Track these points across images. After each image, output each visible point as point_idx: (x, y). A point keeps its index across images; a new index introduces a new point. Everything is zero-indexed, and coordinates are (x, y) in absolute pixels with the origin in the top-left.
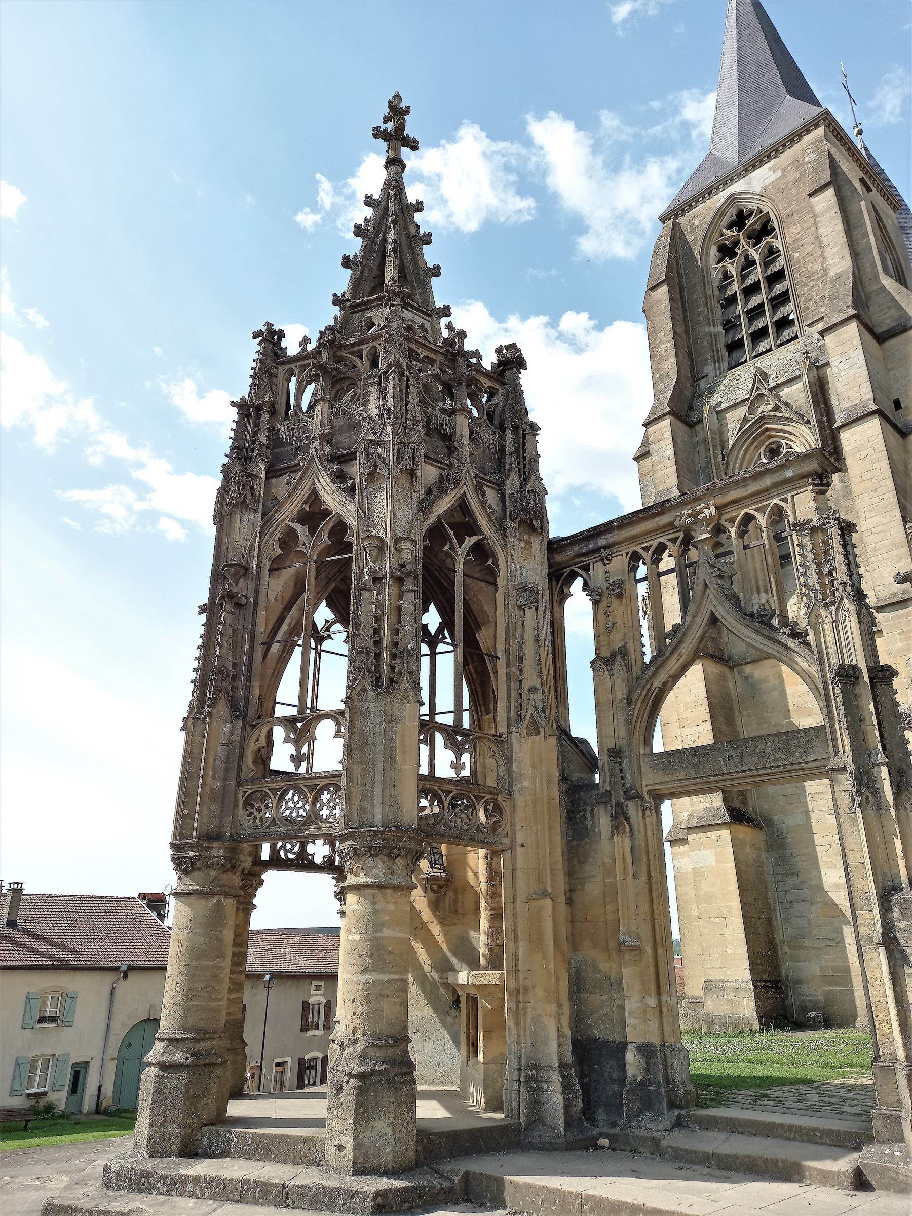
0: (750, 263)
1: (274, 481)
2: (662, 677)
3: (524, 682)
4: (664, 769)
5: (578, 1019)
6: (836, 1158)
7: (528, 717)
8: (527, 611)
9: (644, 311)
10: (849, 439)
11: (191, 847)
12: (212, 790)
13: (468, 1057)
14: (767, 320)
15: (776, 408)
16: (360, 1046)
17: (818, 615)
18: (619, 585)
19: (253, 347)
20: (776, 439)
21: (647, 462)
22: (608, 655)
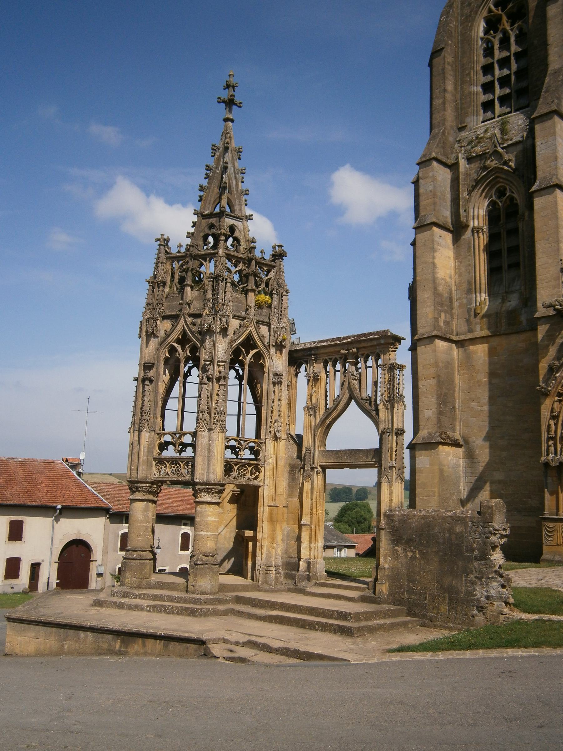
4: (326, 457)
12: (143, 460)
20: (503, 184)
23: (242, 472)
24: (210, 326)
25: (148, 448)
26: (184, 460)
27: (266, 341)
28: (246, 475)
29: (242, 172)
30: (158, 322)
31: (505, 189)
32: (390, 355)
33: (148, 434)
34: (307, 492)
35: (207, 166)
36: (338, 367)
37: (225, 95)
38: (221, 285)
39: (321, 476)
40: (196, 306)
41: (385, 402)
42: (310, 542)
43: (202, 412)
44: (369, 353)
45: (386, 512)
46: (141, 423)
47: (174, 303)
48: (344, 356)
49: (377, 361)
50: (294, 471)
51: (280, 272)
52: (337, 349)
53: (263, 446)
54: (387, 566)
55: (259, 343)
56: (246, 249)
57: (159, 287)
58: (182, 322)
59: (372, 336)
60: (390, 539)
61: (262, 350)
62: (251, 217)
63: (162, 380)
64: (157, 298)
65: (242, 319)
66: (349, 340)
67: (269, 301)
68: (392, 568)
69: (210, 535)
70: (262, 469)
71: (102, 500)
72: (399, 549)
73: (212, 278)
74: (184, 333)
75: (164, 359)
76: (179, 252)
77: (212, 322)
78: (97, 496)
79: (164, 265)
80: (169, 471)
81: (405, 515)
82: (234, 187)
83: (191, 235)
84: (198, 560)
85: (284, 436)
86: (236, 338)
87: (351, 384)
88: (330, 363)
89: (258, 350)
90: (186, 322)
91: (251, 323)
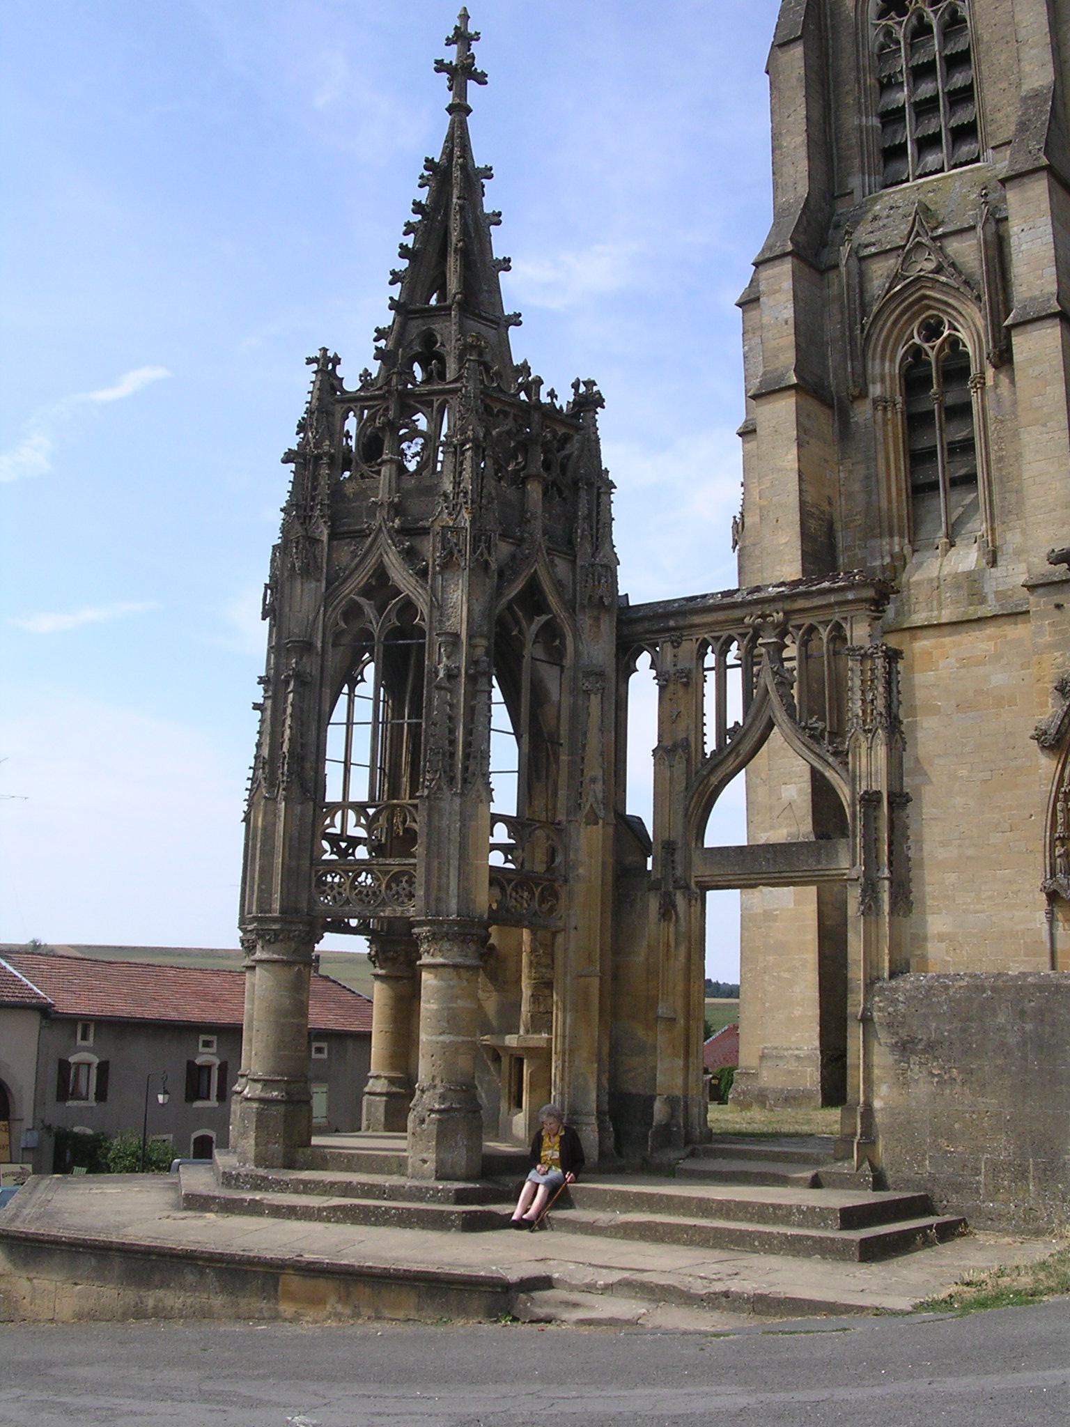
0: (922, 29)
1: (335, 543)
2: (720, 774)
5: (614, 1078)
6: (804, 1171)
7: (588, 807)
8: (592, 696)
9: (767, 72)
10: (1023, 344)
11: (274, 920)
13: (510, 1108)
14: (941, 122)
15: (939, 270)
16: (440, 1090)
17: (857, 740)
18: (687, 674)
19: (306, 377)
20: (935, 312)
21: (754, 314)
22: (670, 743)
31: (941, 323)
37: (451, 55)
44: (816, 624)
48: (751, 630)
52: (737, 613)
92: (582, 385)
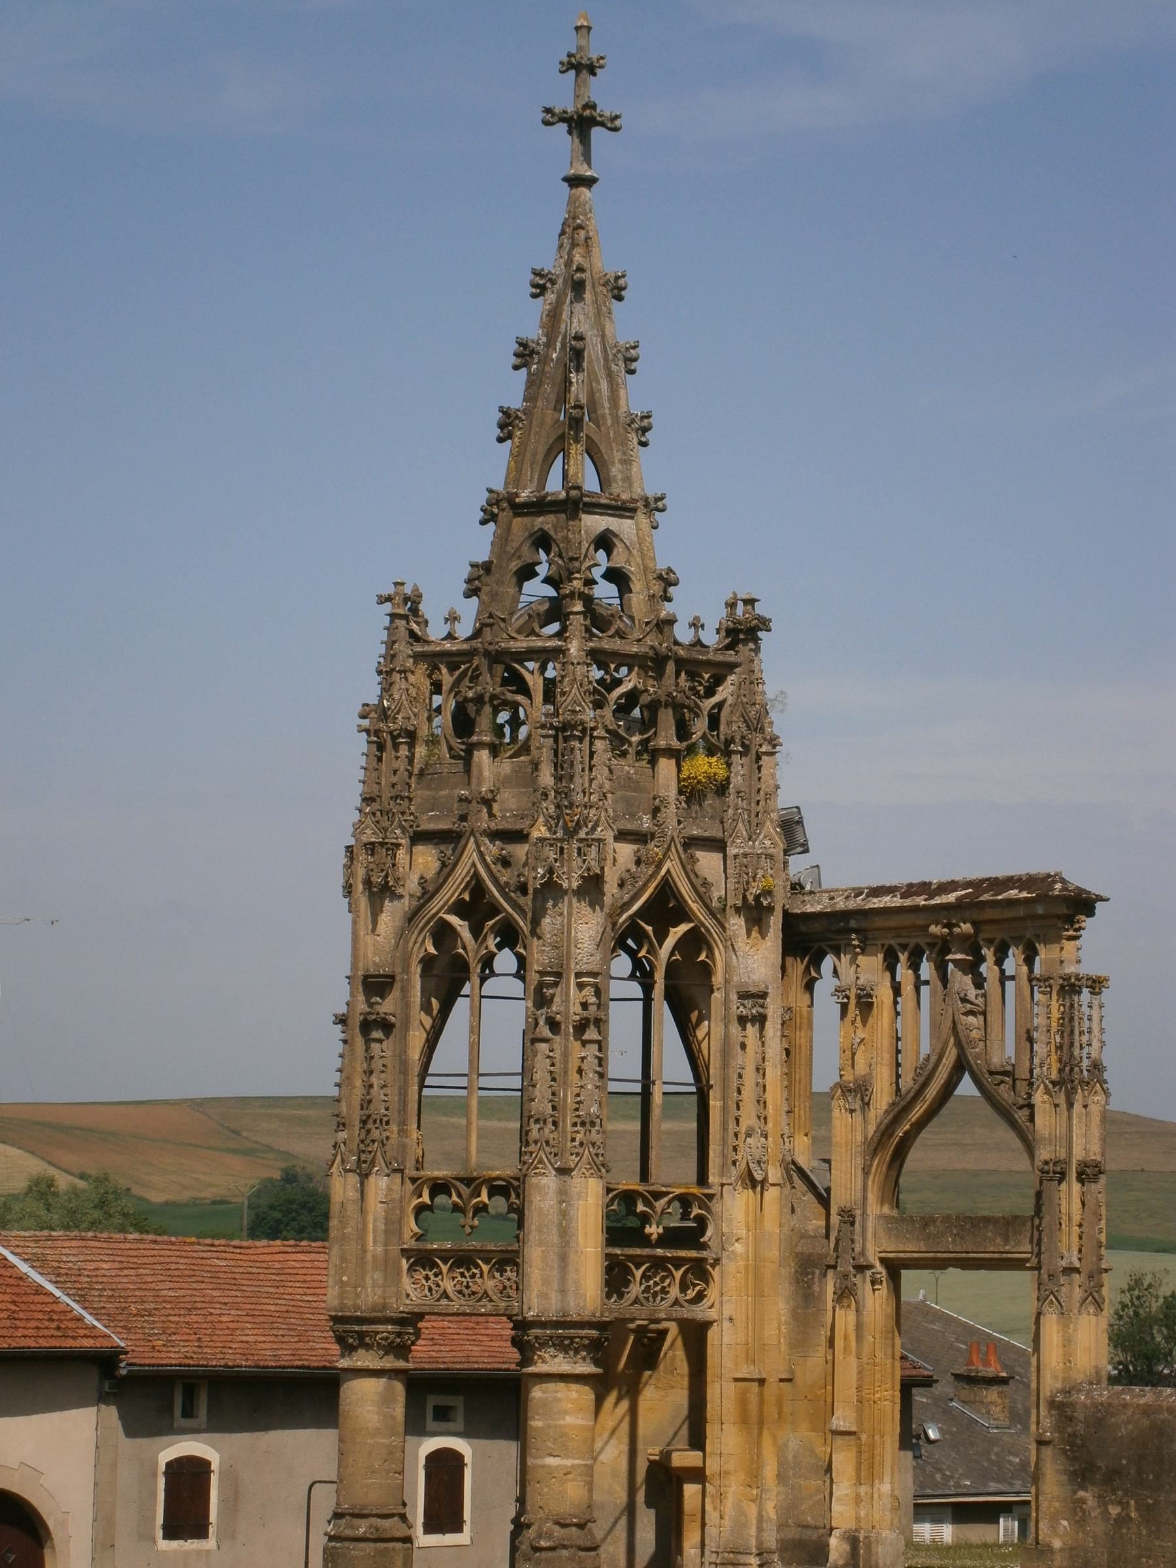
3: (741, 1120)
4: (897, 1237)
8: (749, 1025)
23: (656, 1284)
24: (551, 871)
25: (387, 1221)
26: (491, 1255)
27: (717, 893)
28: (668, 1292)
29: (628, 355)
30: (401, 854)
32: (1062, 949)
33: (383, 1182)
34: (846, 1338)
35: (520, 344)
36: (927, 969)
38: (580, 749)
39: (884, 1290)
40: (509, 803)
41: (1050, 1086)
42: (859, 1482)
43: (537, 1121)
44: (1007, 939)
45: (1053, 1396)
46: (363, 1152)
47: (442, 793)
49: (1029, 962)
50: (808, 1274)
51: (753, 681)
53: (715, 1205)
54: (1057, 1544)
55: (694, 906)
56: (647, 624)
57: (396, 747)
58: (470, 855)
59: (1013, 893)
60: (1065, 1470)
61: (703, 925)
62: (660, 504)
63: (418, 1022)
64: (394, 779)
65: (640, 838)
66: (951, 898)
67: (721, 773)
68: (1071, 1549)
69: (572, 1466)
70: (716, 1273)
71: (80, 1319)
72: (1088, 1496)
73: (552, 727)
74: (477, 887)
75: (420, 962)
76: (450, 636)
77: (556, 860)
78: (56, 1301)
79: (410, 676)
80: (448, 1285)
81: (1102, 1404)
82: (607, 405)
83: (482, 572)
84: (540, 1536)
85: (774, 1174)
86: (626, 897)
87: (960, 1027)
88: (903, 957)
89: (692, 925)
90: (481, 855)
91: (669, 848)
92: (740, 604)
